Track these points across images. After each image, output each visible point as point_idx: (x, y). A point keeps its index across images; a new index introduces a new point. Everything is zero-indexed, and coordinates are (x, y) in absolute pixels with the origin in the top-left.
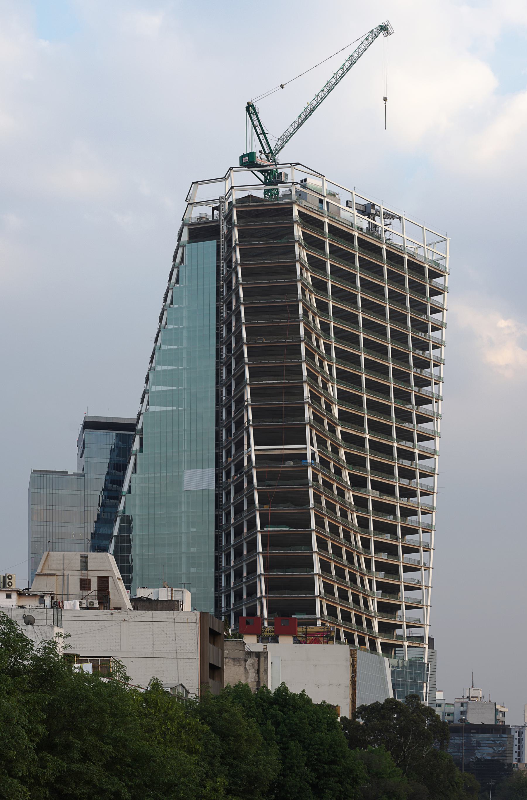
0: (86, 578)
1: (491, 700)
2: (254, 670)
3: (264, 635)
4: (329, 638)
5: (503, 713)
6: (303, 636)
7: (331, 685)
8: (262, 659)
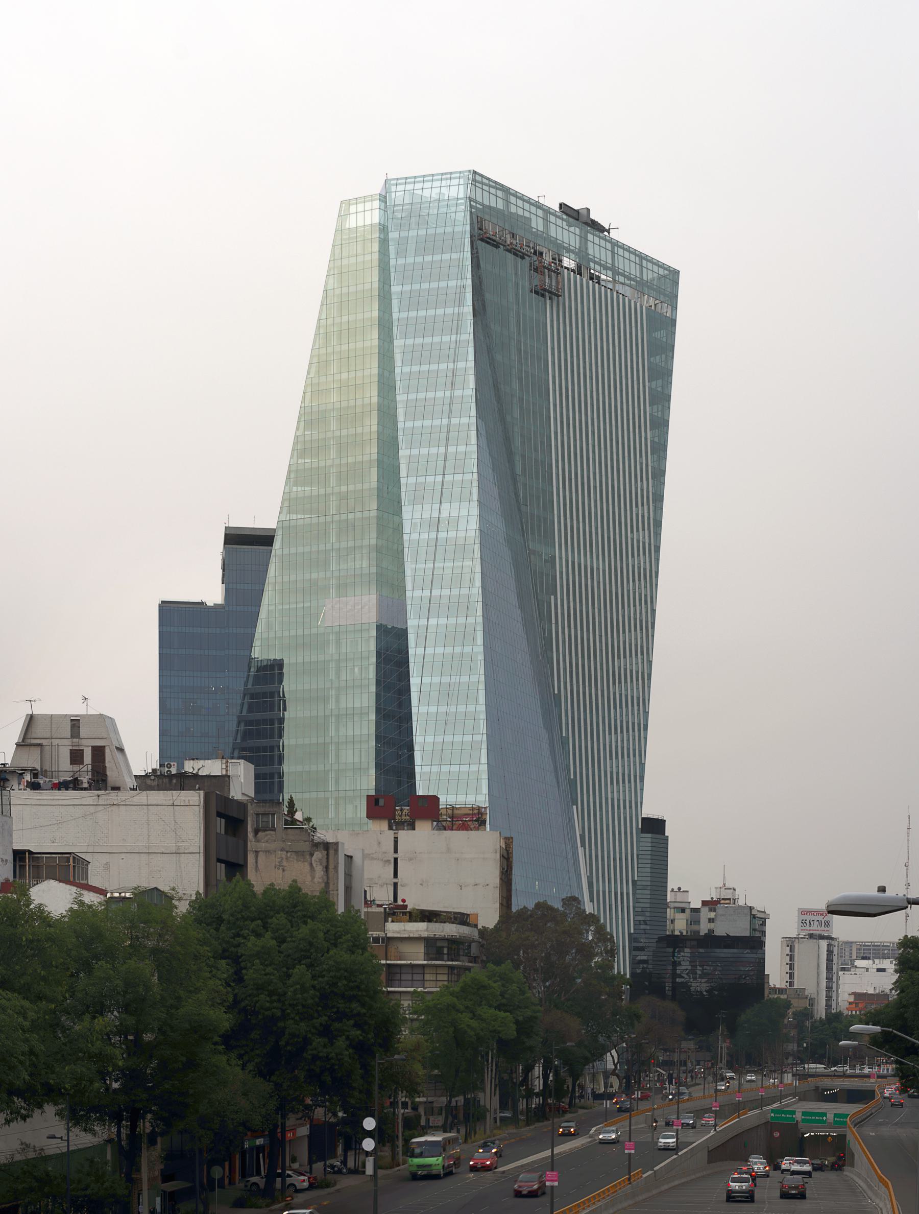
0: (77, 748)
6: (449, 819)
8: (331, 852)
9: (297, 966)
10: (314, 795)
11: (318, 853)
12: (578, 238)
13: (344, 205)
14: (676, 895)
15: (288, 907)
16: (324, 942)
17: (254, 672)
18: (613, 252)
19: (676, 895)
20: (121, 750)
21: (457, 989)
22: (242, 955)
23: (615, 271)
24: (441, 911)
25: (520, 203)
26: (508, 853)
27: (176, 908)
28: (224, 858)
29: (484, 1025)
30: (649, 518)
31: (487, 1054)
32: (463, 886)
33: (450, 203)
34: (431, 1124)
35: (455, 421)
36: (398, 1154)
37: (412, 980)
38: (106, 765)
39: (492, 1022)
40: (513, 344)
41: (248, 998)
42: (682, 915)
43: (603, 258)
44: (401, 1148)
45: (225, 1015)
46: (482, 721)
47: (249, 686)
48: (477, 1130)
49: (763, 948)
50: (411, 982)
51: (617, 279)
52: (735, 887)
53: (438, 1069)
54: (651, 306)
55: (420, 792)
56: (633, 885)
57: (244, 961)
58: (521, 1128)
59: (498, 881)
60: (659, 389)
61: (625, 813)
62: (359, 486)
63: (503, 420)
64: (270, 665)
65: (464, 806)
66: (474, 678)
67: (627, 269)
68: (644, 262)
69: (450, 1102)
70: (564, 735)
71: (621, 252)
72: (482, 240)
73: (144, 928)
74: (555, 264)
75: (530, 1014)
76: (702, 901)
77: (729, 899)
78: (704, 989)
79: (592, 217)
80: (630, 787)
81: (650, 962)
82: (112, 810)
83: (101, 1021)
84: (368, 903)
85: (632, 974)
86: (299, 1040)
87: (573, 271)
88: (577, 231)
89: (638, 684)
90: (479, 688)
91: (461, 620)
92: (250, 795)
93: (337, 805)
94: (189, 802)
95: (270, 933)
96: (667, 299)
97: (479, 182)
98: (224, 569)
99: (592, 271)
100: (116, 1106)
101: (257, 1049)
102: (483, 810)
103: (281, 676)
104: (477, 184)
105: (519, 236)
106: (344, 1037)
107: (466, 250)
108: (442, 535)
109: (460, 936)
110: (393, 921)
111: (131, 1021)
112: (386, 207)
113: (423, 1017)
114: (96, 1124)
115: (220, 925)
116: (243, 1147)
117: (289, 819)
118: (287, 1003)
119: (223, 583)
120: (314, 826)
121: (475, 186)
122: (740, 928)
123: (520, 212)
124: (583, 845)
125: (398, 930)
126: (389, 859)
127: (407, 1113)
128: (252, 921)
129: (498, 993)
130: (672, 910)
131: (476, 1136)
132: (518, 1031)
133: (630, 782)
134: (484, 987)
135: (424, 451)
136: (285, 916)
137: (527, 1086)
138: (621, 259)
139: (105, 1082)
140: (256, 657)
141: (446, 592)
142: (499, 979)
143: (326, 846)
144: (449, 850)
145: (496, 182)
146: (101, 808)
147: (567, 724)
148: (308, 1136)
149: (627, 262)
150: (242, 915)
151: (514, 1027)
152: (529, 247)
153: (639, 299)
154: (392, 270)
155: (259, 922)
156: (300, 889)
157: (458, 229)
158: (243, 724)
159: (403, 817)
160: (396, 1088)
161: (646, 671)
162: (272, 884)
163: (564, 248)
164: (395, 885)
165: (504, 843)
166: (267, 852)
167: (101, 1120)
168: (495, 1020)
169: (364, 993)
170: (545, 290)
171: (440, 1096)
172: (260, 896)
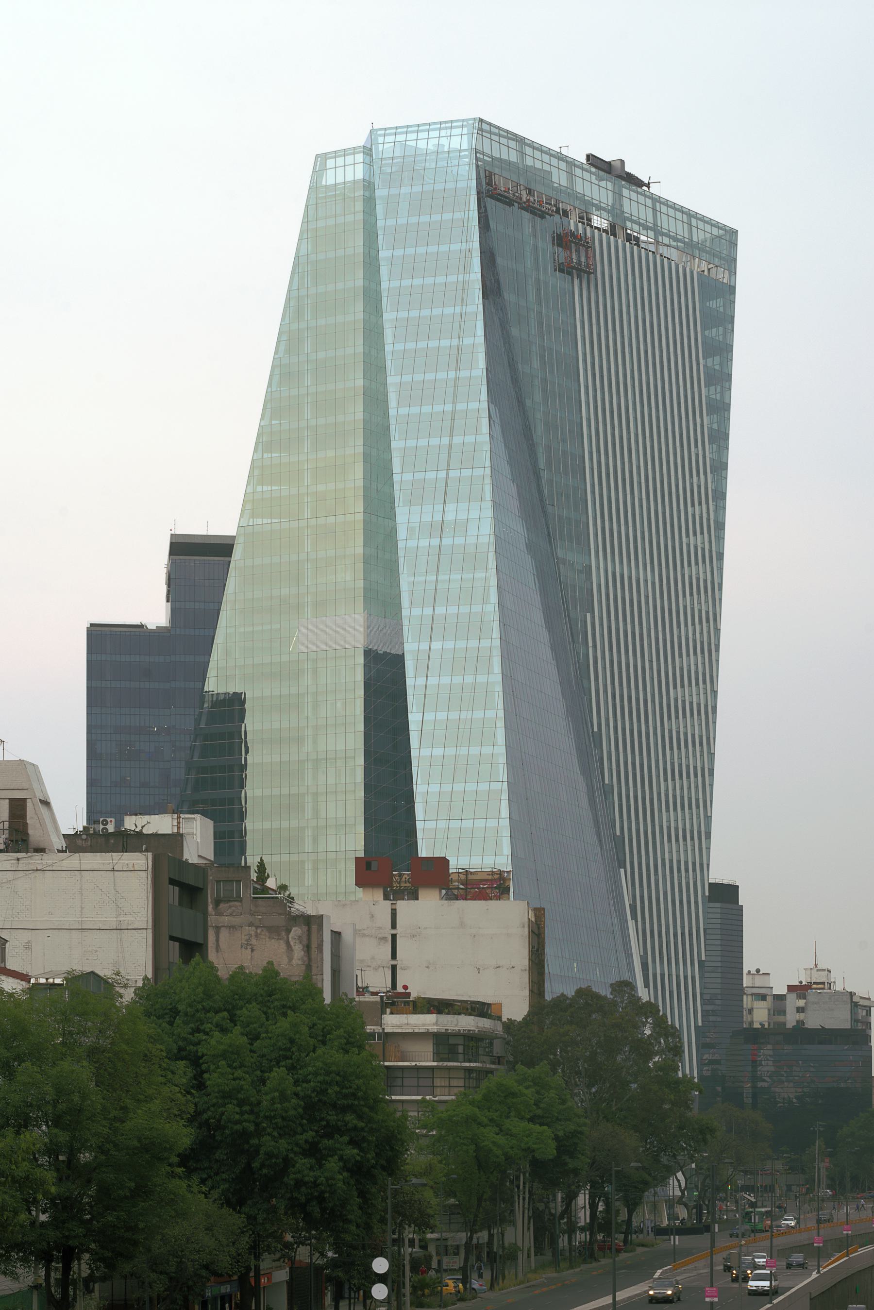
1: (846, 988)
2: (301, 946)
3: (401, 887)
5: (868, 1009)
6: (461, 887)
7: (499, 967)
8: (314, 928)
9: (274, 1069)
10: (285, 858)
12: (610, 193)
14: (753, 979)
15: (262, 996)
18: (654, 209)
19: (753, 979)
20: (46, 803)
21: (478, 1097)
22: (203, 1055)
23: (657, 231)
24: (454, 1000)
25: (538, 154)
26: (539, 928)
29: (514, 1142)
30: (708, 520)
31: (518, 1178)
32: (481, 968)
33: (451, 155)
34: (445, 1267)
35: (461, 406)
36: (404, 1303)
37: (418, 1086)
38: (28, 822)
39: (525, 1138)
41: (212, 1109)
43: (643, 216)
44: (409, 1298)
45: (184, 1130)
47: (203, 725)
52: (829, 968)
53: (455, 1196)
54: (704, 271)
55: (423, 852)
57: (207, 1063)
60: (717, 367)
61: (687, 877)
63: (520, 402)
65: (480, 870)
66: (490, 714)
67: (672, 229)
68: (694, 221)
70: (607, 782)
71: (664, 209)
72: (491, 197)
73: (80, 1021)
75: (573, 1127)
76: (788, 986)
77: (823, 983)
79: (627, 169)
80: (693, 846)
83: (28, 1136)
84: (362, 991)
85: (701, 1077)
86: (278, 1161)
87: (604, 231)
88: (610, 186)
89: (700, 719)
90: (497, 726)
93: (316, 869)
94: (134, 866)
96: (723, 262)
99: (629, 231)
100: (44, 1243)
101: (223, 1173)
102: (506, 874)
103: (243, 712)
104: (484, 134)
105: (537, 191)
106: (336, 1157)
108: (447, 541)
110: (392, 1013)
111: (63, 1137)
112: (372, 161)
114: (18, 1265)
115: (175, 1018)
117: (259, 887)
118: (262, 1114)
119: (168, 601)
122: (840, 1019)
123: (538, 165)
126: (386, 936)
128: (216, 1012)
129: (532, 1102)
130: (749, 997)
131: (505, 1281)
132: (558, 1149)
133: (692, 839)
134: (514, 1095)
135: (423, 442)
136: (258, 1006)
137: (569, 1218)
138: (664, 217)
139: (30, 1213)
142: (532, 1084)
144: (462, 925)
145: (507, 131)
146: (21, 874)
147: (610, 769)
149: (672, 220)
150: (202, 1006)
151: (553, 1144)
152: (550, 204)
153: (689, 263)
154: (380, 232)
156: (277, 974)
157: (461, 185)
160: (402, 1221)
161: (709, 703)
162: (242, 968)
163: (593, 205)
164: (394, 968)
166: (232, 928)
167: (25, 1260)
169: (362, 1103)
170: (573, 268)
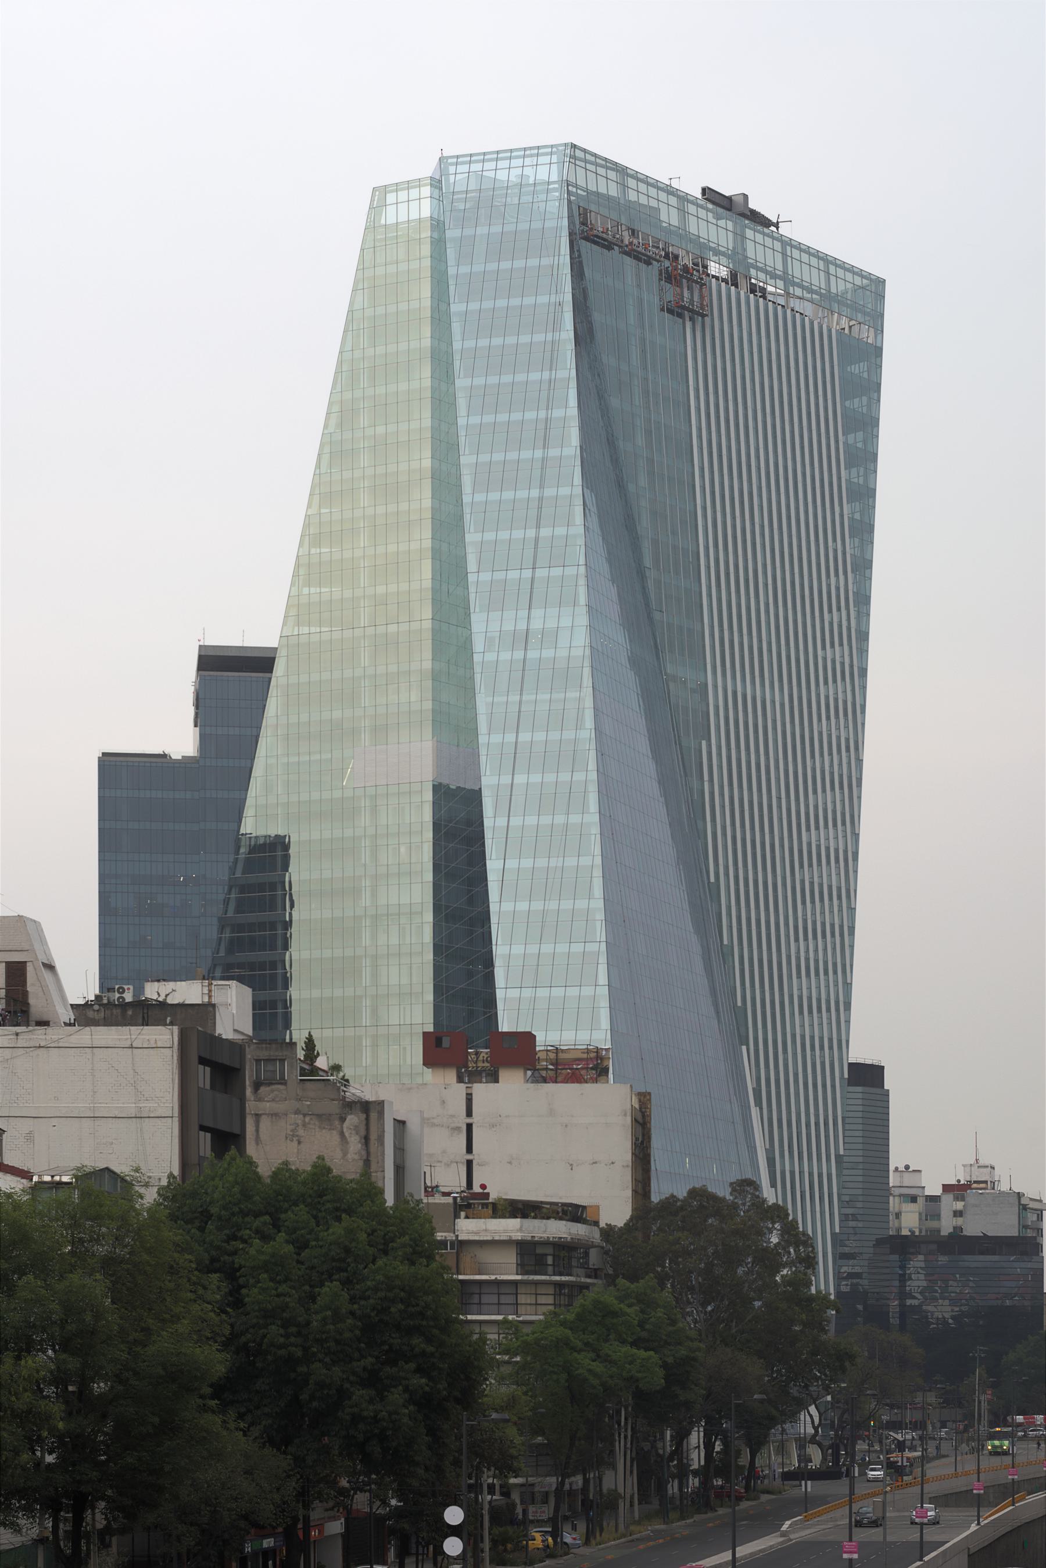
1: (1013, 1188)
2: (357, 1138)
3: (477, 1067)
4: (599, 1070)
6: (551, 1067)
7: (595, 1163)
8: (373, 1115)
9: (326, 1283)
10: (339, 1032)
11: (353, 1116)
13: (377, 193)
14: (901, 1177)
15: (310, 1196)
16: (368, 1247)
17: (244, 853)
18: (784, 254)
19: (901, 1177)
20: (50, 967)
22: (240, 1268)
24: (542, 1202)
25: (642, 187)
26: (644, 1116)
27: (142, 1198)
28: (211, 1124)
31: (619, 1412)
32: (575, 1165)
33: (538, 188)
34: (531, 1518)
35: (549, 492)
37: (499, 1304)
38: (28, 989)
39: (627, 1365)
40: (636, 383)
41: (251, 1330)
42: (912, 1207)
43: (770, 262)
44: (488, 1554)
46: (598, 924)
47: (238, 874)
48: (605, 1524)
49: (1040, 1254)
50: (496, 1307)
51: (791, 291)
52: (993, 1164)
53: (543, 1434)
54: (844, 329)
55: (505, 1025)
56: (836, 1162)
57: (244, 1276)
58: (673, 1523)
59: (628, 1157)
60: (860, 445)
62: (404, 587)
64: (269, 843)
65: (573, 1047)
66: (586, 861)
67: (806, 278)
69: (562, 1483)
70: (725, 942)
71: (796, 253)
73: (92, 1226)
74: (698, 271)
75: (685, 1353)
76: (943, 1185)
77: (986, 1182)
78: (947, 1315)
79: (751, 205)
80: (830, 1019)
81: (864, 1275)
82: (38, 1055)
83: (30, 1362)
84: (431, 1190)
87: (723, 280)
88: (730, 225)
89: (838, 868)
90: (594, 875)
91: (564, 777)
92: (246, 1032)
93: (375, 1046)
95: (284, 1234)
96: (867, 318)
97: (580, 160)
98: (197, 706)
99: (753, 281)
101: (265, 1405)
104: (578, 162)
106: (401, 1388)
107: (562, 252)
108: (532, 654)
109: (572, 1238)
110: (467, 1217)
111: (73, 1363)
113: (518, 1359)
114: (20, 1515)
115: (206, 1223)
116: (242, 1551)
119: (196, 726)
120: (346, 1078)
121: (575, 165)
122: (1006, 1225)
123: (643, 200)
124: (758, 1103)
125: (475, 1230)
126: (459, 1125)
127: (496, 1500)
128: (256, 1216)
130: (897, 1199)
133: (828, 1010)
134: (614, 1314)
136: (307, 1209)
137: (680, 1460)
138: (796, 264)
139: (34, 1453)
140: (248, 832)
141: (540, 736)
143: (366, 1107)
145: (606, 160)
146: (21, 1051)
148: (341, 1533)
150: (239, 1208)
151: (661, 1373)
152: (658, 248)
153: (826, 320)
154: (451, 282)
155: (267, 1218)
156: (329, 1170)
158: (228, 930)
159: (480, 1064)
162: (286, 1163)
163: (711, 249)
164: (469, 1164)
165: (637, 1100)
166: (274, 1115)
167: (28, 1510)
168: (631, 1363)
169: (431, 1323)
170: (684, 308)
171: (546, 1476)
172: (268, 1181)
